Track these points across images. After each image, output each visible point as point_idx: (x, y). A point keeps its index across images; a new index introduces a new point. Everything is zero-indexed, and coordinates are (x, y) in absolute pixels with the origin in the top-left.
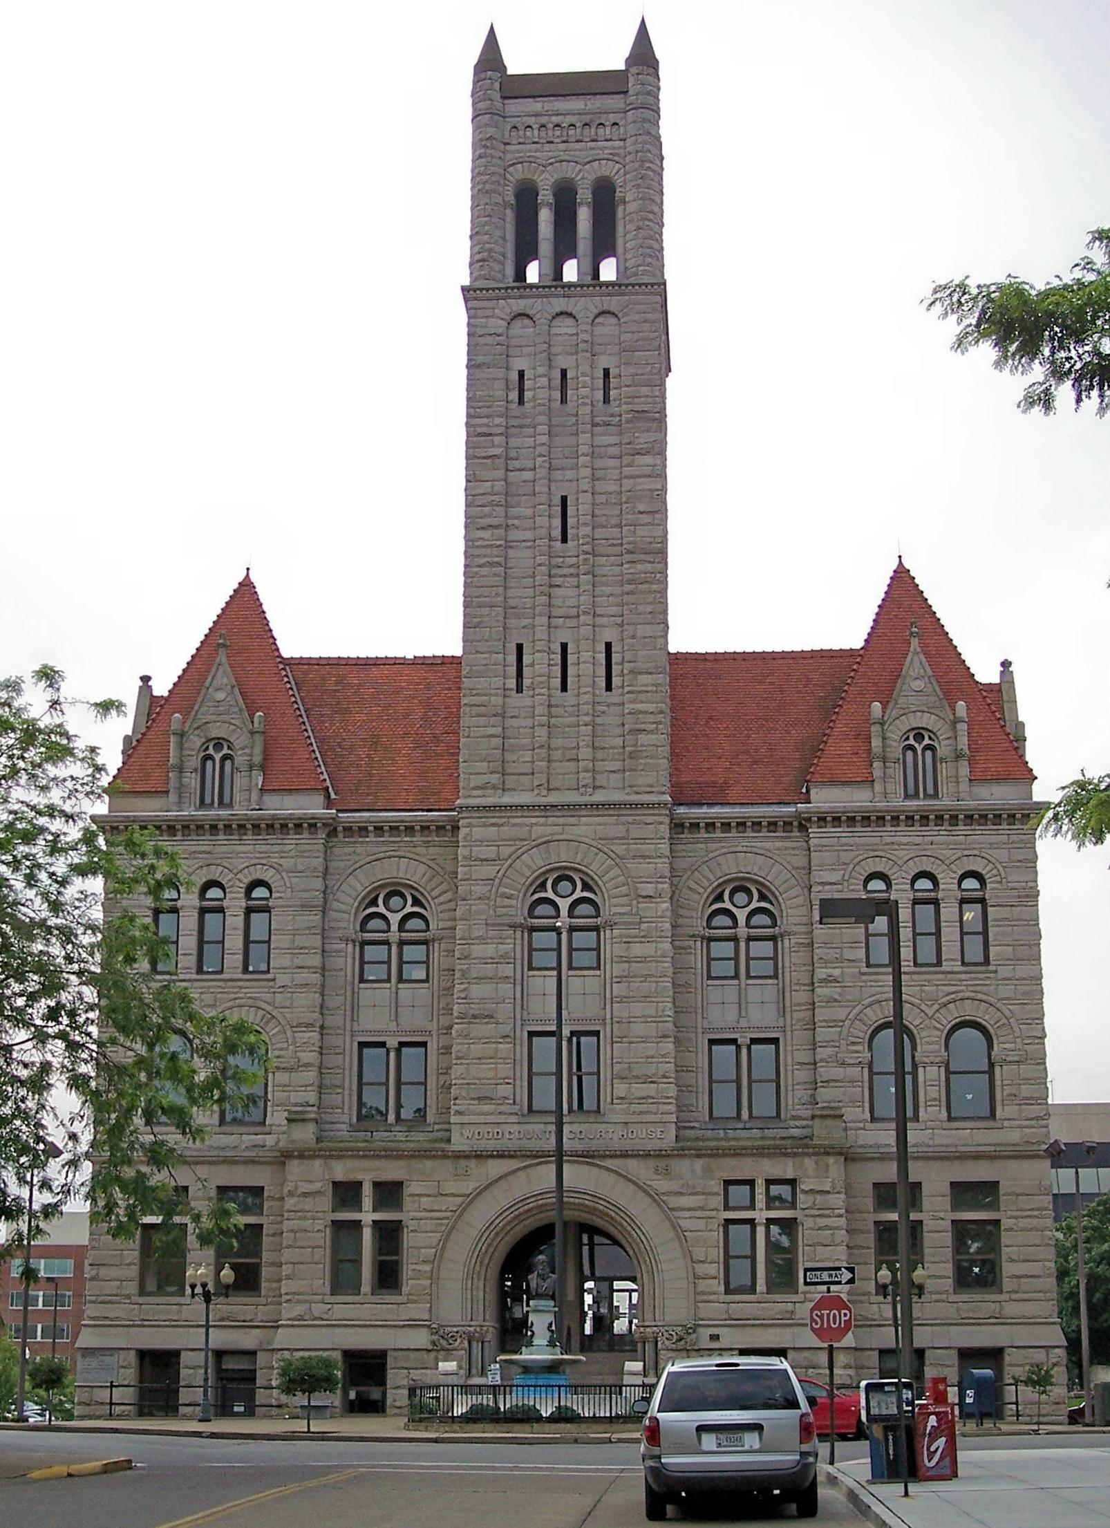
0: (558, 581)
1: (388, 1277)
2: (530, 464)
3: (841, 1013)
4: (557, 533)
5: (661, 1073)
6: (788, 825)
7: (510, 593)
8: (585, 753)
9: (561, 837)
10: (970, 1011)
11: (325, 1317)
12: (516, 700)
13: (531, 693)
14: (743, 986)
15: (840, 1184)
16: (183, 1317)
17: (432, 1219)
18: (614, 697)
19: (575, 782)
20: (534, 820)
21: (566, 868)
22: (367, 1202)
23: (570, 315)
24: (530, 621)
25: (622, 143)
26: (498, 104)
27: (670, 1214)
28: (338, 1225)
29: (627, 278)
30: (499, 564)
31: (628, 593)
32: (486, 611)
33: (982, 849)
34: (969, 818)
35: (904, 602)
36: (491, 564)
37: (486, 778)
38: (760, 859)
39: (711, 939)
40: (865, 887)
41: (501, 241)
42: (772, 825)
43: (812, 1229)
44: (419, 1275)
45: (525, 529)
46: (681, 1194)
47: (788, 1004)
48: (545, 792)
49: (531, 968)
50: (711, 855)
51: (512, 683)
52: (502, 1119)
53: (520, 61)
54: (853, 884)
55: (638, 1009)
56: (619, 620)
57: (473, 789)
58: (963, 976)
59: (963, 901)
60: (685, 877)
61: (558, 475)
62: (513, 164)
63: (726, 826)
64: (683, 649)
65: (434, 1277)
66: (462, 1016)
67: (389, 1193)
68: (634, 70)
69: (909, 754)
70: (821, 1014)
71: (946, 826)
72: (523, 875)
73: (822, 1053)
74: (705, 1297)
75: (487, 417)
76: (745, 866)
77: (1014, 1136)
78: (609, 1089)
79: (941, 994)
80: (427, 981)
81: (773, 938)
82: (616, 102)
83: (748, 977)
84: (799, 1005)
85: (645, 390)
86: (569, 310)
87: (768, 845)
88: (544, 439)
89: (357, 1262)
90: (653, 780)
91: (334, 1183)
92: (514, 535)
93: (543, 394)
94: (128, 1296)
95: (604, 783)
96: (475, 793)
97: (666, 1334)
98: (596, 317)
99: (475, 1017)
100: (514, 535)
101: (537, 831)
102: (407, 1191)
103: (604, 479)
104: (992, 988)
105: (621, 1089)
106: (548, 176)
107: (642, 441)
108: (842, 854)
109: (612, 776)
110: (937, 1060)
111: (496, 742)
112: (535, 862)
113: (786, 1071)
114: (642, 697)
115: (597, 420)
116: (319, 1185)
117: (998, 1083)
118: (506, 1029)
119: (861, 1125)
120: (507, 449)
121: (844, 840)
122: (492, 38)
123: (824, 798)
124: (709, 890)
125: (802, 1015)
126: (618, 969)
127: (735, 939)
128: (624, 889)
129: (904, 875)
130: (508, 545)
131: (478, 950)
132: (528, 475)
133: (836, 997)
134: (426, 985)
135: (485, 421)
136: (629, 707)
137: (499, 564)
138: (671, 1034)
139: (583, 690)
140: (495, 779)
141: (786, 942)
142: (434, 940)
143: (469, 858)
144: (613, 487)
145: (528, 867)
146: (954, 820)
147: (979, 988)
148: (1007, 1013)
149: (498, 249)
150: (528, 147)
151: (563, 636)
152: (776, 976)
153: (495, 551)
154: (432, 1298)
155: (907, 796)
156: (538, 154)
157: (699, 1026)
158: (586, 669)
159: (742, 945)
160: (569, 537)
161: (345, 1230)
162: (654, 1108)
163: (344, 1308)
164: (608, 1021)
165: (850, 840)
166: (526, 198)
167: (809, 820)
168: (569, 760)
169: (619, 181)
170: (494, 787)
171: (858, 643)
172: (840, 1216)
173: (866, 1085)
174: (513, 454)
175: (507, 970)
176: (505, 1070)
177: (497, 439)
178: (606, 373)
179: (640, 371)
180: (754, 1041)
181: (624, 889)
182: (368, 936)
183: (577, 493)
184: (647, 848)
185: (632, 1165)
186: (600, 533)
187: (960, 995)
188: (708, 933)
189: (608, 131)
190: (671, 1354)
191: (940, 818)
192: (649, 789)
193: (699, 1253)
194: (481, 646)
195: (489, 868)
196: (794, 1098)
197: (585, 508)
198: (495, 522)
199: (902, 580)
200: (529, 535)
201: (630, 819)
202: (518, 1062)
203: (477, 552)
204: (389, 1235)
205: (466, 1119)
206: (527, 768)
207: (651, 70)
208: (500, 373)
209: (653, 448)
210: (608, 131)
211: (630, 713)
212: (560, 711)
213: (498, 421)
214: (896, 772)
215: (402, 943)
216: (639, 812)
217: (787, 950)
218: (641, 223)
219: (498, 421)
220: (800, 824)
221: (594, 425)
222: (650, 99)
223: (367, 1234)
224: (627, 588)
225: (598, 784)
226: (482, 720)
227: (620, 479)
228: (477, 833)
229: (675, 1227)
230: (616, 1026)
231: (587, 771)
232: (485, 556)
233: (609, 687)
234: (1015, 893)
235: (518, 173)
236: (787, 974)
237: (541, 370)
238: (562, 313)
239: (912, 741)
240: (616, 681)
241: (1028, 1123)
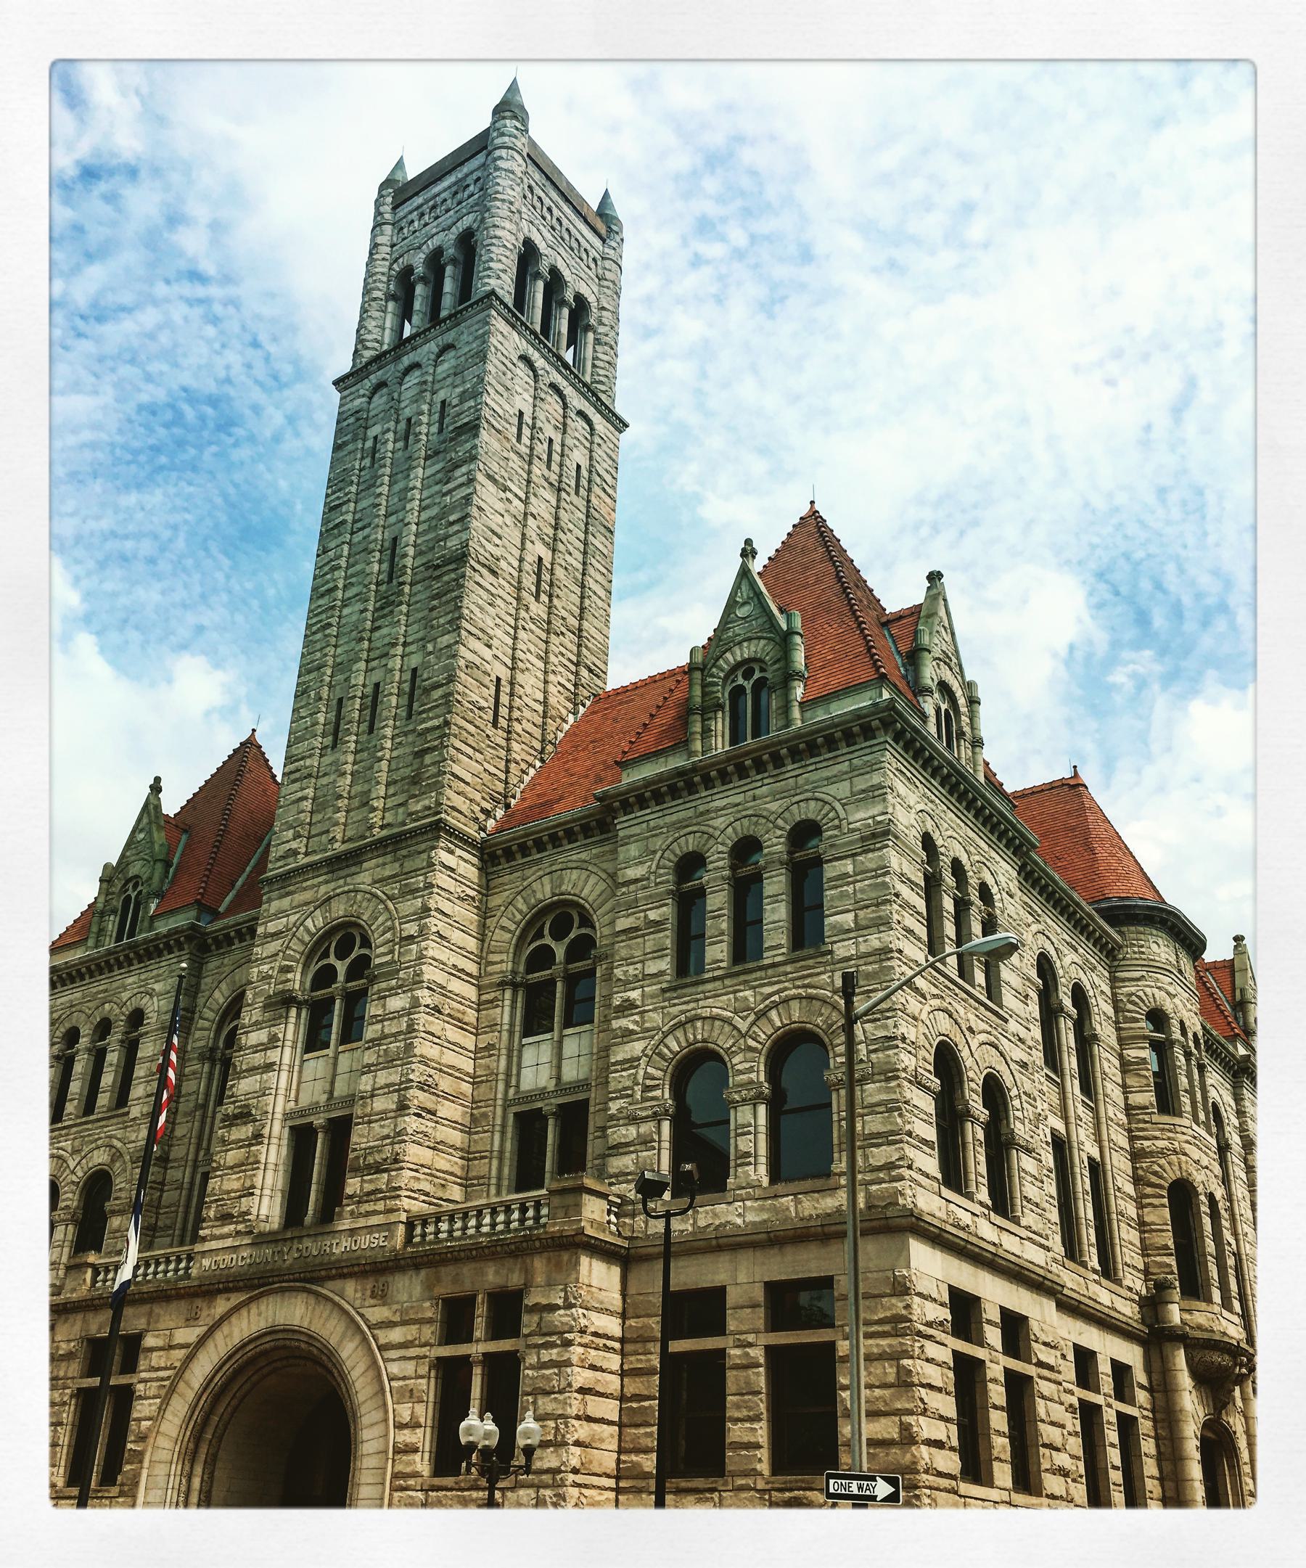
54: (661, 875)
64: (1019, 787)
87: (583, 856)
98: (439, 356)
129: (721, 848)
146: (778, 761)
165: (661, 822)
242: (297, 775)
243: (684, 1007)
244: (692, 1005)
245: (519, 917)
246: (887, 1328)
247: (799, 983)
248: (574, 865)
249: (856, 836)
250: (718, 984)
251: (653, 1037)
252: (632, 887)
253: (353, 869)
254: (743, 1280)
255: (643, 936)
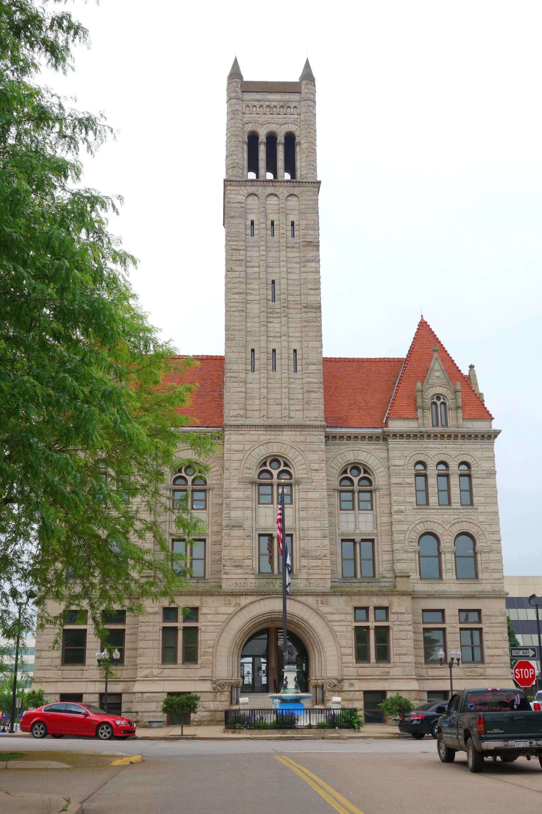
0: (271, 320)
1: (191, 656)
2: (257, 264)
3: (405, 527)
4: (270, 297)
5: (323, 554)
6: (378, 438)
7: (248, 325)
8: (285, 401)
9: (273, 441)
10: (465, 527)
11: (160, 675)
12: (251, 376)
13: (259, 372)
14: (357, 514)
15: (410, 610)
16: (84, 677)
17: (213, 626)
18: (298, 375)
19: (280, 415)
20: (261, 432)
21: (277, 455)
22: (180, 617)
23: (276, 195)
24: (258, 338)
25: (298, 116)
26: (240, 95)
27: (328, 623)
28: (165, 630)
29: (302, 179)
30: (243, 311)
31: (304, 327)
32: (237, 333)
33: (472, 451)
34: (463, 436)
35: (425, 335)
36: (239, 311)
37: (237, 412)
38: (365, 454)
39: (341, 491)
40: (415, 467)
41: (242, 159)
42: (371, 438)
43: (397, 631)
44: (206, 654)
45: (255, 295)
46: (334, 613)
47: (379, 522)
48: (266, 419)
49: (259, 503)
50: (341, 452)
51: (249, 367)
52: (247, 576)
53: (249, 75)
54: (409, 466)
55: (312, 524)
56: (300, 339)
57: (231, 417)
58: (462, 511)
59: (461, 475)
60: (330, 461)
61: (270, 270)
62: (247, 123)
63: (349, 438)
65: (214, 655)
66: (227, 526)
67: (193, 613)
68: (304, 82)
69: (434, 406)
70: (395, 528)
71: (452, 440)
72: (256, 458)
73: (397, 546)
74: (346, 665)
75: (237, 241)
76: (357, 457)
77: (488, 588)
78: (298, 562)
79: (451, 519)
80: (205, 509)
81: (371, 492)
82: (295, 97)
83: (359, 509)
84: (385, 523)
85: (312, 232)
86: (275, 193)
87: (368, 447)
88: (264, 253)
89: (175, 648)
90: (316, 414)
91: (163, 608)
92: (250, 297)
93: (263, 232)
94: (56, 666)
95: (294, 416)
96: (232, 419)
97: (328, 683)
99: (233, 526)
100: (250, 297)
101: (262, 438)
102: (201, 611)
103: (292, 273)
104: (475, 516)
105: (304, 562)
106: (264, 130)
107: (310, 256)
108: (404, 452)
109: (297, 412)
110: (451, 550)
111: (242, 395)
112: (263, 452)
113: (378, 555)
114: (312, 375)
115: (289, 245)
116: (157, 609)
117: (479, 562)
118: (248, 533)
119: (416, 581)
120: (246, 256)
121: (405, 446)
122: (236, 63)
123: (395, 426)
124: (341, 468)
125: (385, 528)
126: (303, 504)
127: (352, 492)
128: (304, 466)
129: (433, 462)
130: (247, 302)
131: (234, 494)
132: (256, 270)
133: (403, 519)
134: (205, 511)
135: (235, 243)
136: (306, 380)
137: (243, 311)
138: (328, 536)
139: (283, 371)
140: (242, 412)
141: (377, 493)
142: (209, 490)
143: (229, 450)
144: (296, 277)
145: (258, 454)
146: (456, 436)
147: (469, 517)
148: (483, 529)
149: (241, 162)
150: (254, 115)
151: (273, 346)
152: (372, 509)
153: (241, 305)
154: (212, 665)
155: (433, 426)
156: (259, 119)
157: (337, 532)
158: (285, 361)
159: (356, 494)
160: (276, 299)
161: (169, 633)
162: (320, 572)
163: (170, 671)
164: (298, 529)
166: (253, 138)
167: (388, 435)
168: (277, 404)
169: (297, 133)
170: (242, 416)
171: (403, 354)
172: (410, 625)
173: (418, 562)
174: (249, 259)
175: (249, 504)
176: (247, 553)
177: (241, 252)
178: (293, 224)
179: (310, 223)
180: (363, 540)
181: (304, 466)
182: (177, 487)
183: (280, 278)
184: (315, 447)
185: (310, 600)
186: (290, 298)
187: (461, 520)
188: (340, 488)
189: (292, 110)
190: (331, 693)
191: (449, 436)
192: (316, 419)
193: (343, 643)
194: (235, 349)
195: (239, 454)
196: (382, 568)
197: (284, 286)
198: (241, 291)
199: (423, 326)
200: (257, 298)
201: (306, 433)
202: (254, 549)
203: (232, 305)
204: (192, 634)
205: (229, 576)
206: (257, 408)
207: (312, 83)
208: (243, 221)
209: (315, 259)
210: (292, 110)
211: (306, 383)
212: (273, 381)
213: (242, 243)
214: (428, 414)
215: (193, 491)
216: (311, 429)
217: (378, 497)
218: (308, 154)
219: (242, 243)
220: (384, 438)
221: (287, 247)
222: (312, 96)
223: (180, 634)
224: (304, 324)
225: (291, 416)
226: (236, 385)
227: (300, 273)
228: (234, 438)
229: (331, 629)
230: (301, 531)
231: (286, 409)
232: (236, 307)
233: (296, 371)
234: (485, 472)
235: (249, 128)
236: (378, 509)
237: (262, 220)
238: (271, 194)
239: (435, 400)
240: (299, 368)
241: (494, 581)
242: (236, 379)
243: (423, 516)
244: (426, 516)
245: (340, 465)
246: (500, 625)
247: (465, 517)
248: (364, 450)
249: (485, 472)
250: (435, 511)
251: (411, 525)
252: (397, 468)
253: (279, 433)
254: (452, 608)
255: (404, 487)
